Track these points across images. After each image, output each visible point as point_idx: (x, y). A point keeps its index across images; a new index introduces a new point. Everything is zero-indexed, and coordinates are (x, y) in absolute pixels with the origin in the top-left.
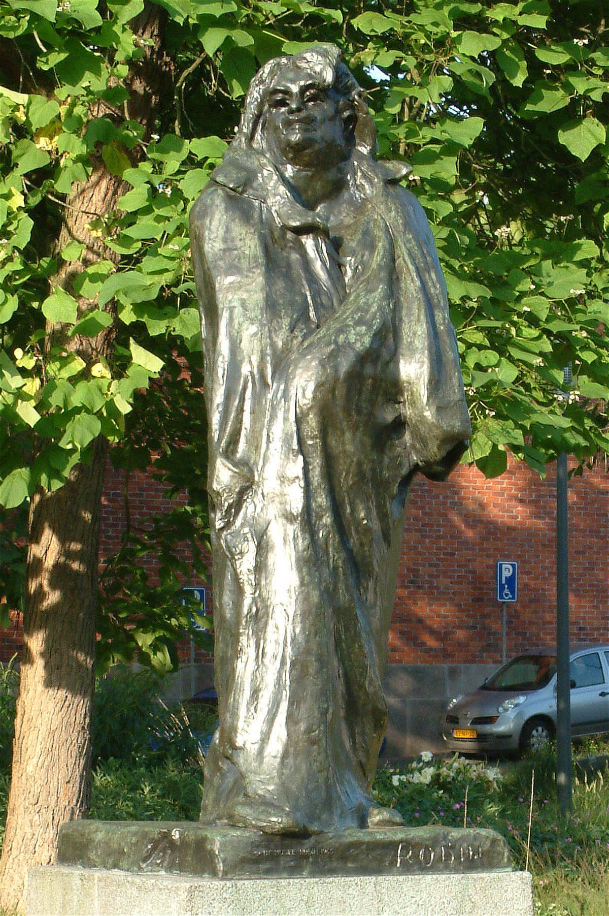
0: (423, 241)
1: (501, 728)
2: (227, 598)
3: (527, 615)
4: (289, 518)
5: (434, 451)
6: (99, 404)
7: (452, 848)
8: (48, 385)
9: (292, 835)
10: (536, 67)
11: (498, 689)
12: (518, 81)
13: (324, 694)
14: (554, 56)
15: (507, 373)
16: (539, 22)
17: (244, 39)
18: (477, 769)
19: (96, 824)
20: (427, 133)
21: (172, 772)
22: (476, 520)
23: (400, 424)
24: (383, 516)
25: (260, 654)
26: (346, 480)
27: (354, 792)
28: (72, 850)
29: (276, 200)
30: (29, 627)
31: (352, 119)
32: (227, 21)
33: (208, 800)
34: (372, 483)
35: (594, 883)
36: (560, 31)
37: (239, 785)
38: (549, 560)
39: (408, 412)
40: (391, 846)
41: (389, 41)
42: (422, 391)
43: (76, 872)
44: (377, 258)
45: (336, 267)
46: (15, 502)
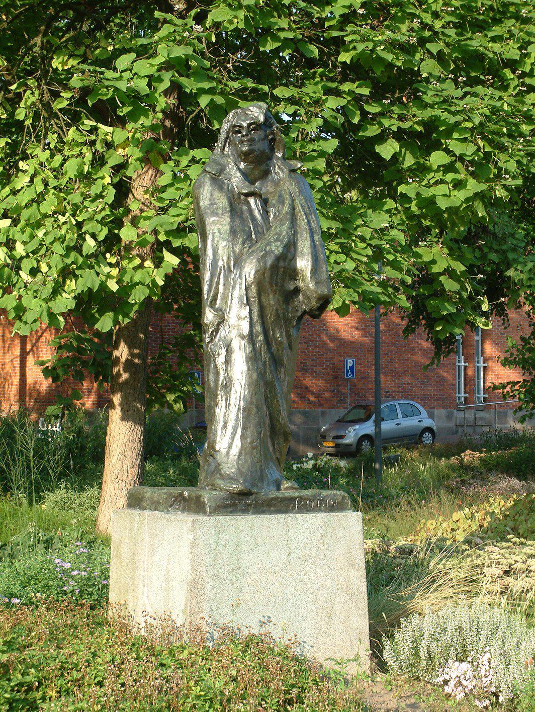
0: (308, 200)
1: (347, 441)
2: (211, 377)
3: (360, 385)
4: (242, 337)
5: (314, 304)
7: (322, 500)
8: (123, 271)
9: (244, 494)
10: (364, 114)
11: (345, 422)
12: (356, 121)
13: (259, 424)
14: (373, 109)
16: (366, 91)
17: (220, 100)
18: (335, 461)
20: (310, 147)
21: (184, 463)
22: (335, 338)
23: (297, 291)
24: (289, 336)
25: (228, 404)
26: (270, 318)
27: (274, 473)
28: (134, 502)
29: (236, 179)
30: (113, 391)
31: (273, 140)
32: (211, 91)
33: (202, 477)
34: (283, 320)
35: (393, 518)
37: (217, 469)
38: (371, 358)
39: (301, 284)
40: (292, 499)
42: (308, 274)
43: (137, 512)
44: (286, 209)
46: (106, 329)
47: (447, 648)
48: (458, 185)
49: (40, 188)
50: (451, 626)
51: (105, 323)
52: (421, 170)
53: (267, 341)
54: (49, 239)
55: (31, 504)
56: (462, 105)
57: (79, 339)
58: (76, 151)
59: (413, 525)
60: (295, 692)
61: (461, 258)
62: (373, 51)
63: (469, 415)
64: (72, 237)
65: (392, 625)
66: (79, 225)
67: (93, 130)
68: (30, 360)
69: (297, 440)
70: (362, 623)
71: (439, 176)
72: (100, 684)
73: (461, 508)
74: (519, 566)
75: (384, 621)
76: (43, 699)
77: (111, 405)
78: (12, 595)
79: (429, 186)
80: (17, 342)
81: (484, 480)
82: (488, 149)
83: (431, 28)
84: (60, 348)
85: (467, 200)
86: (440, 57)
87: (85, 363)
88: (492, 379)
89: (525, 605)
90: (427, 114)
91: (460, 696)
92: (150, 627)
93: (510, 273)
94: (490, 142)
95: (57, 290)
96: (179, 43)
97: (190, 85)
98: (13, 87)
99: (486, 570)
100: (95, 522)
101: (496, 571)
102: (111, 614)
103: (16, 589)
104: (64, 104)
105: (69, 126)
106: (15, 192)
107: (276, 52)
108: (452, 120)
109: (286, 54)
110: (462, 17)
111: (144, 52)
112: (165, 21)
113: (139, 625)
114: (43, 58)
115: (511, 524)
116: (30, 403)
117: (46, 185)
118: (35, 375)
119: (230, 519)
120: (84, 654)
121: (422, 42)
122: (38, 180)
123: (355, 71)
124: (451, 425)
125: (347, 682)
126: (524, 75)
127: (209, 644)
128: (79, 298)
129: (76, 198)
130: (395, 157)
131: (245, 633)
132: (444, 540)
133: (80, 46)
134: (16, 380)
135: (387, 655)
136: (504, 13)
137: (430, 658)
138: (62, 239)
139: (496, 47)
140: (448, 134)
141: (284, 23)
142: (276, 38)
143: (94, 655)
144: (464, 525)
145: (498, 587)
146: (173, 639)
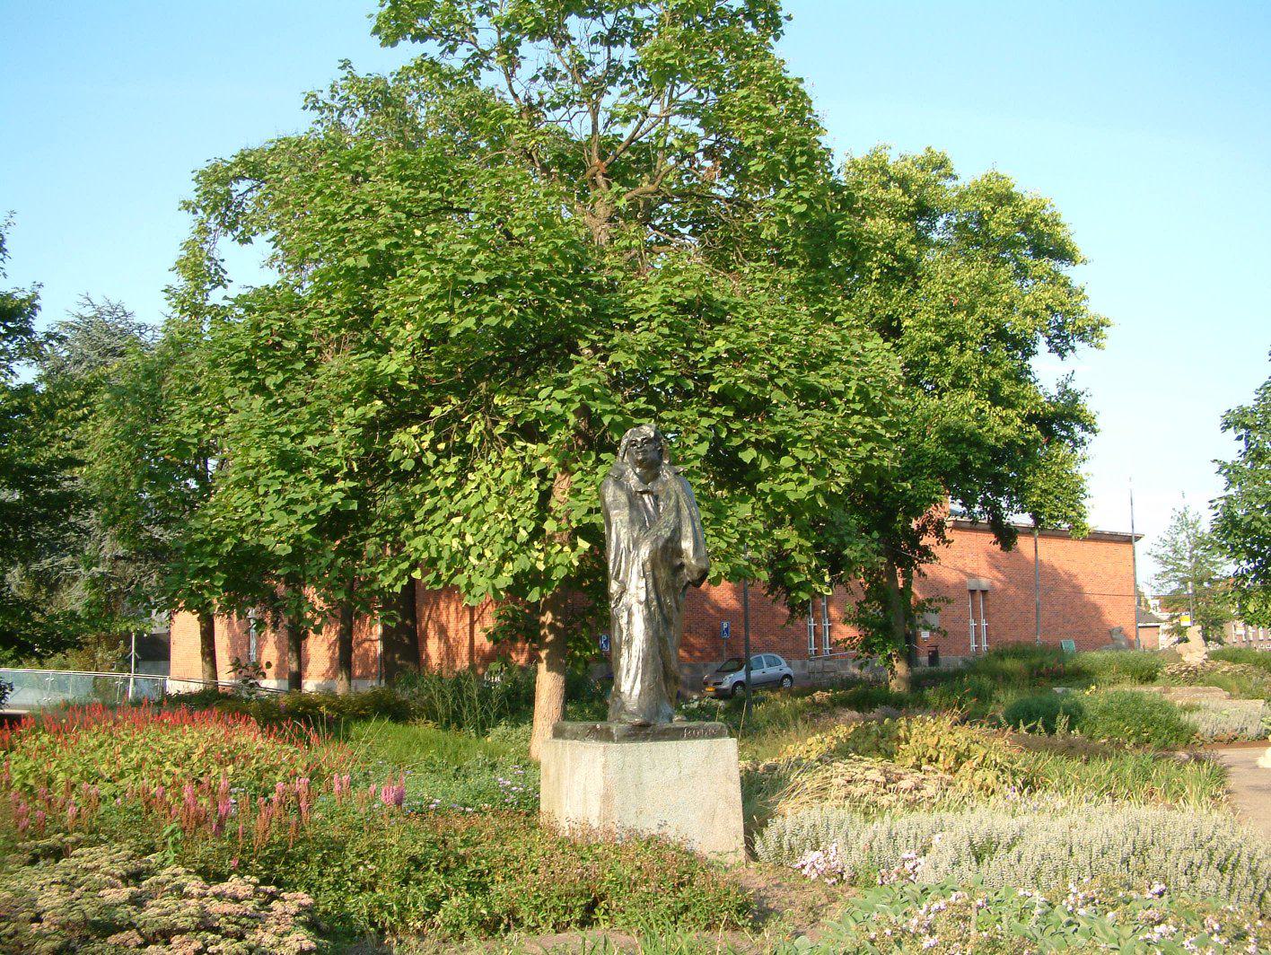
0: (689, 495)
1: (724, 687)
2: (617, 634)
3: (733, 643)
4: (640, 603)
5: (696, 576)
6: (566, 562)
7: (706, 730)
8: (548, 555)
9: (643, 726)
10: (730, 430)
11: (723, 671)
12: (724, 435)
13: (655, 671)
14: (736, 426)
15: (723, 545)
16: (730, 414)
17: (619, 418)
18: (714, 702)
19: (566, 723)
20: (688, 452)
21: (596, 704)
22: (716, 607)
23: (682, 566)
24: (677, 602)
25: (630, 656)
26: (662, 587)
27: (667, 708)
28: (558, 733)
29: (633, 481)
30: (540, 648)
31: (661, 451)
32: (612, 412)
33: (610, 712)
34: (672, 588)
35: (761, 744)
36: (738, 416)
37: (622, 707)
38: (742, 620)
39: (685, 561)
40: (682, 729)
41: (674, 421)
42: (691, 553)
43: (561, 741)
44: (672, 503)
45: (657, 506)
46: (535, 600)
47: (804, 841)
48: (802, 482)
49: (485, 493)
50: (807, 825)
51: (534, 596)
52: (775, 471)
53: (660, 605)
54: (491, 533)
55: (478, 737)
56: (804, 422)
57: (514, 611)
58: (511, 465)
59: (777, 749)
60: (686, 877)
61: (807, 539)
62: (735, 384)
63: (819, 664)
64: (509, 530)
65: (761, 825)
66: (514, 521)
67: (524, 448)
68: (477, 627)
69: (685, 686)
70: (738, 824)
71: (788, 475)
72: (535, 872)
73: (813, 735)
74: (858, 777)
75: (755, 820)
76: (492, 882)
77: (540, 660)
78: (466, 805)
79: (780, 484)
80: (467, 613)
81: (832, 714)
82: (824, 456)
83: (778, 368)
84: (499, 618)
85: (809, 493)
86: (785, 388)
87: (518, 629)
88: (837, 636)
89: (863, 805)
90: (778, 429)
91: (814, 876)
92: (572, 830)
93: (847, 552)
94: (826, 451)
95: (499, 570)
96: (588, 376)
97: (597, 407)
98: (465, 420)
99: (833, 780)
100: (528, 751)
101: (841, 781)
102: (542, 820)
103: (469, 801)
104: (503, 430)
105: (505, 445)
106: (465, 497)
107: (662, 386)
108: (796, 434)
109: (669, 386)
110: (800, 360)
111: (561, 384)
112: (578, 362)
113: (565, 829)
114: (487, 397)
115: (852, 745)
116: (477, 660)
117: (489, 490)
118: (481, 639)
119: (634, 745)
120: (522, 849)
121: (772, 378)
122: (483, 487)
123: (720, 399)
124: (806, 671)
125: (726, 869)
126: (848, 401)
127: (619, 842)
128: (515, 577)
129: (511, 501)
130: (754, 460)
131: (647, 833)
132: (801, 759)
133: (514, 386)
134: (467, 643)
135: (758, 848)
136: (830, 357)
137: (791, 849)
138: (502, 532)
139: (826, 381)
140: (794, 444)
141: (667, 364)
142: (662, 376)
143: (530, 850)
144: (817, 747)
145: (843, 793)
146: (591, 839)
